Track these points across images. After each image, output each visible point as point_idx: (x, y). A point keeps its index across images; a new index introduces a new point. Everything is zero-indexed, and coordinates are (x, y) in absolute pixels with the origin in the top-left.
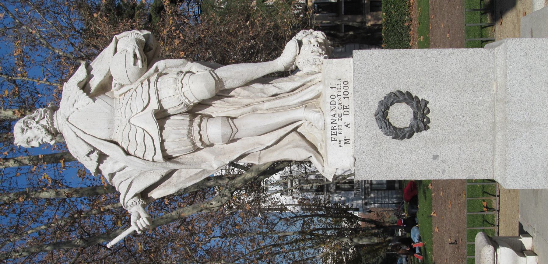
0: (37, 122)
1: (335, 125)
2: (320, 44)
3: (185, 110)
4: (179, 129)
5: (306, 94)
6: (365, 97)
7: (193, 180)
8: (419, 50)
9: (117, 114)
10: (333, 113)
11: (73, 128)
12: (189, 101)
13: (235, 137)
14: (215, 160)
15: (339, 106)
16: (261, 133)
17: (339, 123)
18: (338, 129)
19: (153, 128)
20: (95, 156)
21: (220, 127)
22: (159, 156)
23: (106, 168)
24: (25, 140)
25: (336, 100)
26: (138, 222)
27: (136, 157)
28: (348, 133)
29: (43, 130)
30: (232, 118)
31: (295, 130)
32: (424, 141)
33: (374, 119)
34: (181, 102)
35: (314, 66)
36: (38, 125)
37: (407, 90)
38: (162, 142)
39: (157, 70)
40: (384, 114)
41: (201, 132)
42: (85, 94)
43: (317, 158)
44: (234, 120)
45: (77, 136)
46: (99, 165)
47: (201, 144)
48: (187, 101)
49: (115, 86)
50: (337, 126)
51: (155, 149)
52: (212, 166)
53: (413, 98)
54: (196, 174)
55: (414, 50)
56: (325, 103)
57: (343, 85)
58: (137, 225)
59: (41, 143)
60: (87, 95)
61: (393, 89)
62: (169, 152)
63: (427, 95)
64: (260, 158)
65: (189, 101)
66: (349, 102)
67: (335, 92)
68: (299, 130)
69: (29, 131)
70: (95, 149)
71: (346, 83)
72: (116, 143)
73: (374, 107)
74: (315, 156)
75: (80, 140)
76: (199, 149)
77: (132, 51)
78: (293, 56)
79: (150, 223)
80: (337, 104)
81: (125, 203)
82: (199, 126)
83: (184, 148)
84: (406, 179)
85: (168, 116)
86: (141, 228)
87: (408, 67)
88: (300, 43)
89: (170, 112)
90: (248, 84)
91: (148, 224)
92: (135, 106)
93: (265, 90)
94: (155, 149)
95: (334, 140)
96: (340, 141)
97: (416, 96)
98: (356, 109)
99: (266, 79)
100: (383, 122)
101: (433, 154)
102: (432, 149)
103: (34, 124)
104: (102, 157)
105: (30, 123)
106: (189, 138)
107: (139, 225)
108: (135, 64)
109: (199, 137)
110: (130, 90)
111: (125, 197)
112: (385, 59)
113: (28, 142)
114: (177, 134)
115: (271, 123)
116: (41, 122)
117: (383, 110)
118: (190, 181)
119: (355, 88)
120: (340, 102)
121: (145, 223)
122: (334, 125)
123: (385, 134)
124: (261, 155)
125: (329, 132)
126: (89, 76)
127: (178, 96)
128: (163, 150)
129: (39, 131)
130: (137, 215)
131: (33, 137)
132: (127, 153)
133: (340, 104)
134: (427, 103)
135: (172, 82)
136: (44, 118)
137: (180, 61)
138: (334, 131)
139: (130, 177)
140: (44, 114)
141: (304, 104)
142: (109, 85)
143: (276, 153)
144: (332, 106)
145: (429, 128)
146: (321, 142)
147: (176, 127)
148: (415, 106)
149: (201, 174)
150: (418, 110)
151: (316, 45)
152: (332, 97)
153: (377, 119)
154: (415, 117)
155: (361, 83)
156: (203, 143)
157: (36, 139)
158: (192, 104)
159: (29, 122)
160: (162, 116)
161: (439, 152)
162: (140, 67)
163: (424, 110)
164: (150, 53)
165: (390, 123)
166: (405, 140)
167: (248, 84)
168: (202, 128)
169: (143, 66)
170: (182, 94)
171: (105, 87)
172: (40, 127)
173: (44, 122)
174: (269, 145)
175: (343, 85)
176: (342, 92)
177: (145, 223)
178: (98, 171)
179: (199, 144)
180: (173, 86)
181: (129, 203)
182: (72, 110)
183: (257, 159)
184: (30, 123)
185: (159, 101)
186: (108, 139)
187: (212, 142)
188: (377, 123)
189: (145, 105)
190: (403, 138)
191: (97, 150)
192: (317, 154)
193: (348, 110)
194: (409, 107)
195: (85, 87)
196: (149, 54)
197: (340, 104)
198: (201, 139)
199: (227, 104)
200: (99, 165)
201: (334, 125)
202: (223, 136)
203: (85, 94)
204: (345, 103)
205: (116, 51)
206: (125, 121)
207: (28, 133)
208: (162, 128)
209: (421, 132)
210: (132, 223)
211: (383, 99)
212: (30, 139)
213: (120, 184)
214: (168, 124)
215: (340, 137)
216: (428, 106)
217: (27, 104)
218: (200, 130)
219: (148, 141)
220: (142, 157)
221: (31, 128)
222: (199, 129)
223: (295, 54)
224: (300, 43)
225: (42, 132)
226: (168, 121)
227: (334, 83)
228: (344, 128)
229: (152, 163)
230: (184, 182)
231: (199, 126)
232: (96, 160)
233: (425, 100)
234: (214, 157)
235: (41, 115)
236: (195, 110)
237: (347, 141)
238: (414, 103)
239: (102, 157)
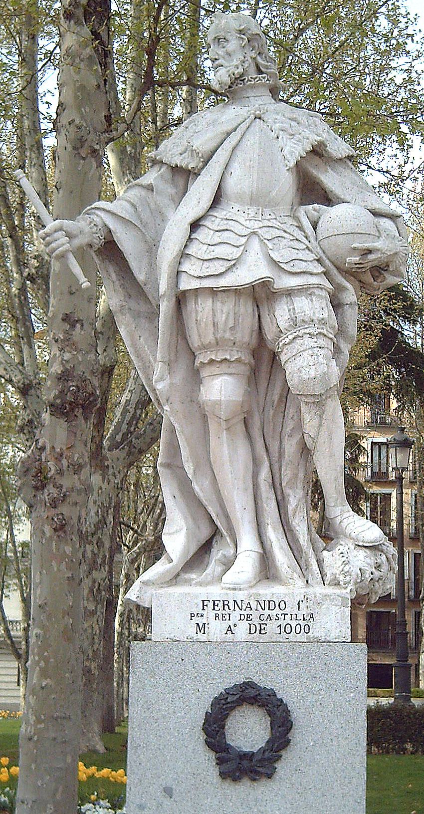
1: (232, 607)
5: (282, 557)
11: (243, 127)
17: (235, 616)
18: (224, 612)
19: (244, 276)
25: (277, 610)
43: (163, 574)
45: (228, 134)
49: (314, 210)
61: (297, 714)
73: (264, 681)
81: (97, 212)
87: (335, 743)
99: (316, 488)
107: (56, 235)
111: (104, 210)
122: (231, 605)
138: (221, 604)
144: (267, 603)
160: (261, 295)
161: (178, 799)
176: (290, 622)
189: (283, 266)
193: (258, 632)
194: (263, 745)
195: (318, 152)
201: (231, 605)
207: (226, 42)
211: (279, 697)
219: (219, 267)
237: (201, 628)
238: (268, 754)
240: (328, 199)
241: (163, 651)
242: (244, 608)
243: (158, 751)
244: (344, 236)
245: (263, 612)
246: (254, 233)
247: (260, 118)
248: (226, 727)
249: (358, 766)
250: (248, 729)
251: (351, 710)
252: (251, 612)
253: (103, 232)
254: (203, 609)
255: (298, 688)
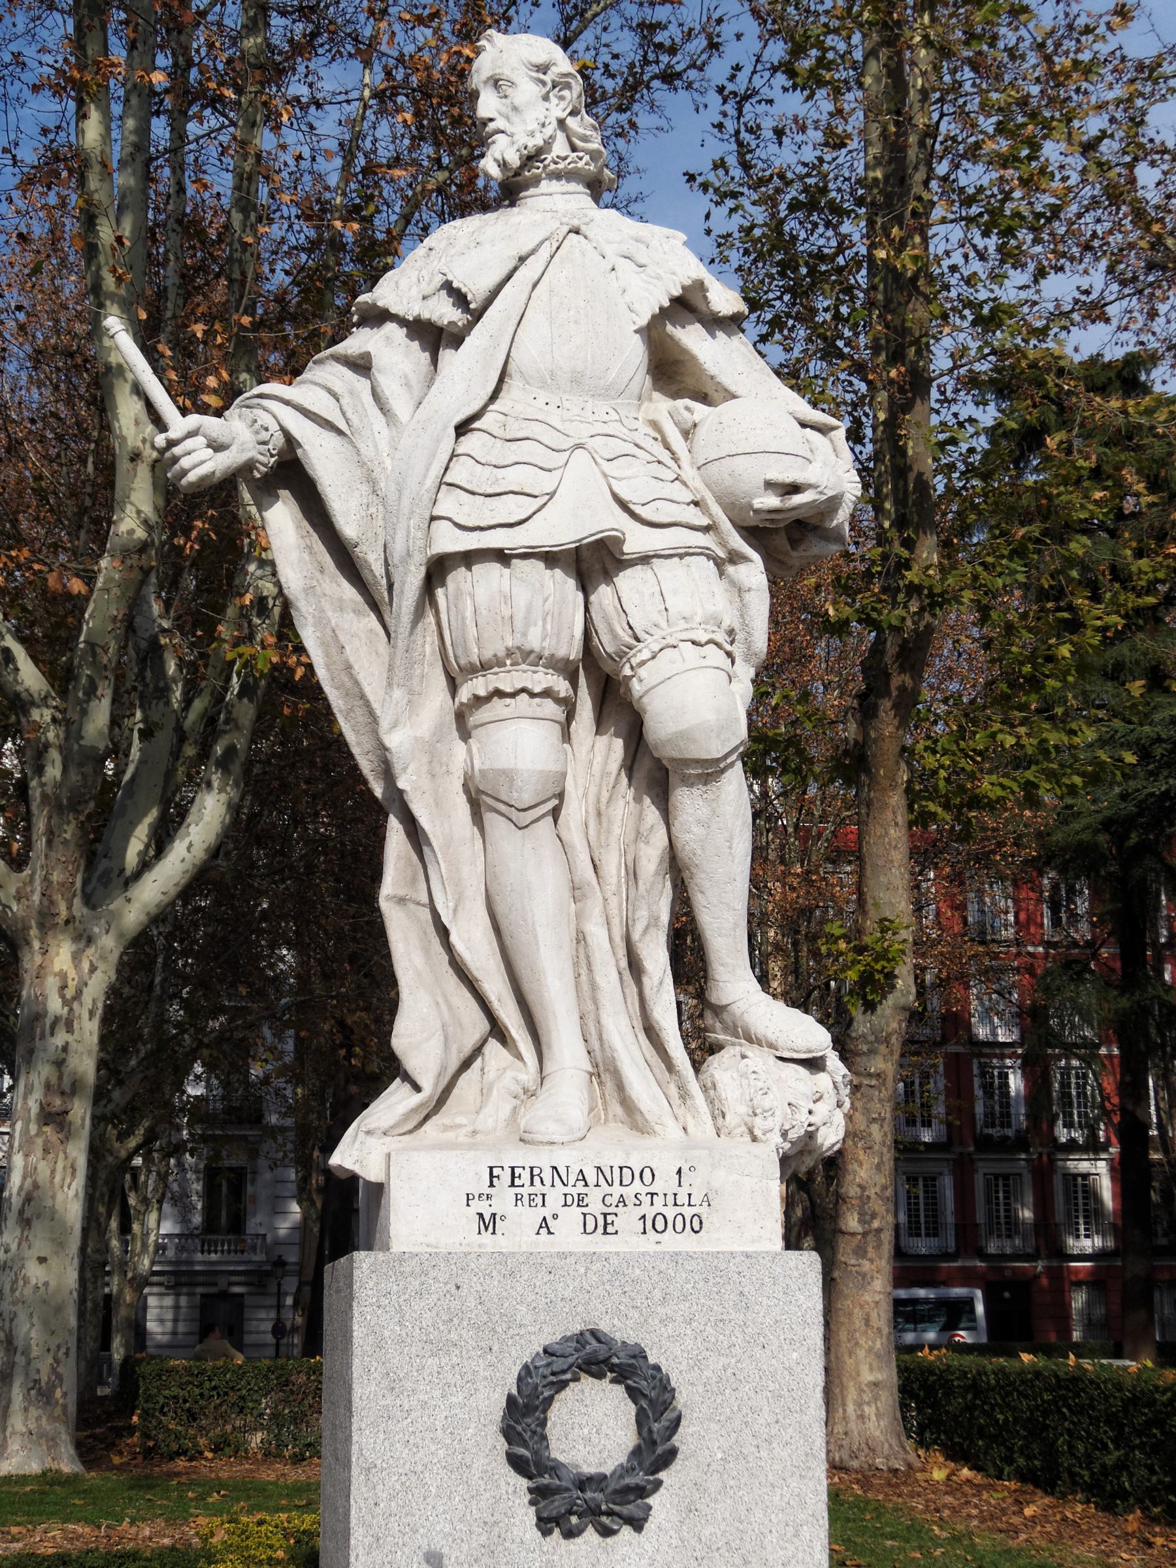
0: (561, 123)
2: (810, 1136)
3: (606, 644)
4: (544, 620)
6: (657, 1294)
7: (327, 655)
8: (825, 1497)
9: (602, 407)
10: (591, 1176)
12: (643, 663)
13: (489, 818)
14: (416, 739)
15: (616, 1197)
16: (500, 910)
17: (555, 1197)
18: (532, 1190)
19: (561, 528)
20: (445, 312)
21: (539, 767)
22: (449, 541)
23: (387, 347)
24: (506, 72)
26: (200, 441)
27: (450, 460)
28: (519, 1228)
29: (539, 141)
30: (555, 813)
31: (498, 1031)
32: (497, 1516)
33: (577, 1328)
34: (641, 635)
35: (743, 1109)
36: (555, 124)
37: (683, 1449)
38: (502, 557)
39: (735, 558)
40: (598, 1363)
41: (524, 696)
42: (666, 304)
44: (550, 819)
45: (522, 260)
46: (402, 321)
47: (482, 693)
48: (645, 655)
49: (687, 409)
50: (544, 1190)
51: (482, 529)
52: (395, 725)
53: (653, 1473)
54: (349, 667)
55: (823, 1476)
56: (613, 1147)
57: (688, 1212)
58: (191, 434)
59: (491, 126)
60: (661, 309)
62: (458, 578)
63: (665, 1525)
64: (401, 901)
65: (643, 663)
66: (629, 1239)
67: (665, 1183)
68: (493, 1045)
69: (538, 90)
70: (478, 315)
71: (696, 1226)
72: (494, 397)
73: (622, 1329)
74: (421, 1106)
75: (510, 266)
76: (453, 686)
77: (813, 481)
78: (772, 1037)
79: (191, 484)
80: (623, 1190)
81: (266, 403)
82: (547, 693)
83: (472, 632)
84: (355, 1448)
85: (585, 587)
86: (177, 450)
87: (764, 1454)
88: (814, 1064)
89: (603, 594)
90: (677, 868)
91: (192, 477)
92: (628, 473)
93: (652, 931)
94: (482, 529)
95: (491, 1176)
96: (489, 1197)
97: (658, 1484)
98: (614, 1260)
100: (571, 1360)
101: (445, 1551)
102: (465, 1547)
103: (558, 109)
104: (434, 338)
105: (562, 98)
106: (509, 653)
107: (189, 444)
108: (769, 485)
109: (509, 690)
110: (675, 459)
111: (287, 403)
112: (790, 1370)
113: (495, 83)
114: (529, 610)
115: (542, 949)
116: (561, 137)
117: (615, 1360)
118: (324, 645)
119: (690, 1256)
120: (631, 1200)
121: (195, 467)
122: (547, 1175)
123: (526, 1367)
124: (412, 906)
125: (522, 1157)
126: (716, 323)
127: (663, 624)
128: (469, 558)
129: (534, 126)
130: (223, 439)
131: (517, 102)
132: (463, 428)
133: (622, 1200)
134: (637, 1524)
135: (711, 609)
136: (574, 149)
137: (761, 642)
138: (526, 1175)
139: (365, 425)
140: (587, 152)
141: (604, 1071)
142: (674, 388)
143: (418, 960)
144: (616, 1171)
145: (546, 1533)
146: (470, 1129)
147: (546, 611)
148: (629, 1481)
149: (349, 684)
150: (616, 1492)
151: (812, 1119)
152: (647, 1174)
153: (579, 1339)
154: (584, 1483)
155: (706, 1281)
156: (479, 701)
157: (508, 111)
158: (627, 671)
159: (566, 93)
160: (594, 562)
162: (758, 503)
163: (610, 1513)
164: (781, 541)
165: (563, 1385)
166: (502, 1445)
167: (677, 868)
168: (537, 700)
169: (756, 511)
170: (671, 641)
171: (669, 371)
172: (549, 131)
173: (560, 147)
174: (454, 938)
175: (688, 1212)
176: (664, 1211)
177: (195, 467)
178: (378, 317)
179: (479, 686)
180: (700, 611)
181: (265, 419)
182: (609, 250)
183: (401, 893)
184: (562, 98)
185: (645, 559)
186: (512, 367)
187: (474, 733)
188: (566, 1339)
189: (638, 509)
190: (508, 1433)
191: (470, 326)
192: (425, 1112)
193: (600, 1229)
195: (686, 306)
196: (783, 535)
197: (622, 1200)
198: (499, 693)
199: (605, 795)
200: (402, 321)
201: (547, 1175)
202: (508, 775)
203: (666, 304)
204: (626, 1220)
205: (804, 425)
206: (581, 433)
207: (522, 84)
208: (550, 559)
209: (532, 1503)
210: (194, 420)
211: (652, 1360)
212: (509, 91)
213: (330, 391)
214: (562, 584)
215: (503, 1200)
216: (626, 1532)
217: (613, 98)
218: (532, 695)
219: (524, 507)
220: (447, 479)
221: (546, 98)
222: (537, 690)
223: (780, 1043)
224: (814, 1064)
225: (532, 134)
226: (571, 583)
227: (696, 1184)
228: (534, 1216)
229: (428, 517)
230: (321, 621)
231: (547, 693)
232: (426, 315)
233: (645, 1520)
234: (427, 736)
235: (585, 139)
236: (604, 686)
237: (488, 1223)
238: (639, 1478)
239: (434, 338)
240: (706, 393)
241: (417, 1270)
242: (571, 1182)
243: (414, 1478)
244: (520, 435)
245: (609, 1190)
246: (579, 446)
247: (577, 232)
248: (549, 1424)
249: (811, 1499)
250: (590, 1432)
251: (794, 1385)
252: (584, 1190)
253: (279, 440)
254: (492, 1185)
255: (689, 1343)
